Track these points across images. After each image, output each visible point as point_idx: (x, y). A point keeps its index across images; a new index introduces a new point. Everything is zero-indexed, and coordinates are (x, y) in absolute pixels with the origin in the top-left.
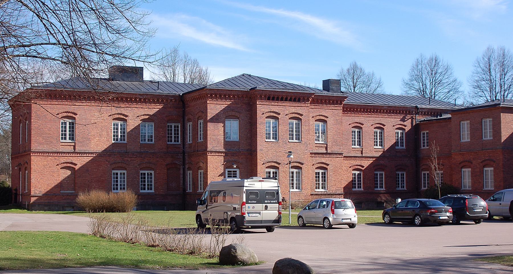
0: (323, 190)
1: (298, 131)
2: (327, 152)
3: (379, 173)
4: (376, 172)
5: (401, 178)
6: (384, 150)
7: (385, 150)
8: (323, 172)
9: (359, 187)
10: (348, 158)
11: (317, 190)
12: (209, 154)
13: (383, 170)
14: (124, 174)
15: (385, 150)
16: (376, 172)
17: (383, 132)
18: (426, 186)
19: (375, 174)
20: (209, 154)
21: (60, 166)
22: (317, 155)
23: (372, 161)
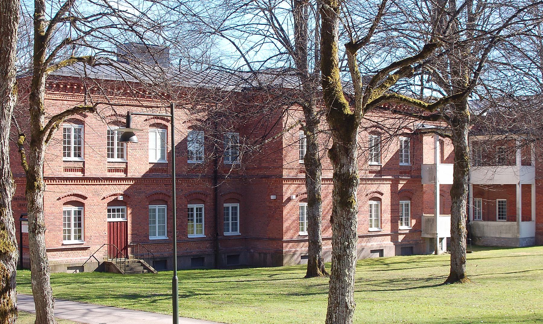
0: (77, 242)
1: (78, 142)
2: (84, 176)
3: (195, 206)
4: (190, 206)
5: (197, 216)
6: (381, 167)
7: (382, 167)
8: (78, 210)
9: (234, 229)
10: (99, 182)
11: (66, 242)
12: (284, 182)
13: (237, 201)
14: (201, 209)
15: (382, 167)
16: (190, 206)
17: (83, 130)
18: (478, 215)
19: (225, 207)
20: (284, 182)
21: (369, 196)
22: (89, 182)
23: (128, 186)
